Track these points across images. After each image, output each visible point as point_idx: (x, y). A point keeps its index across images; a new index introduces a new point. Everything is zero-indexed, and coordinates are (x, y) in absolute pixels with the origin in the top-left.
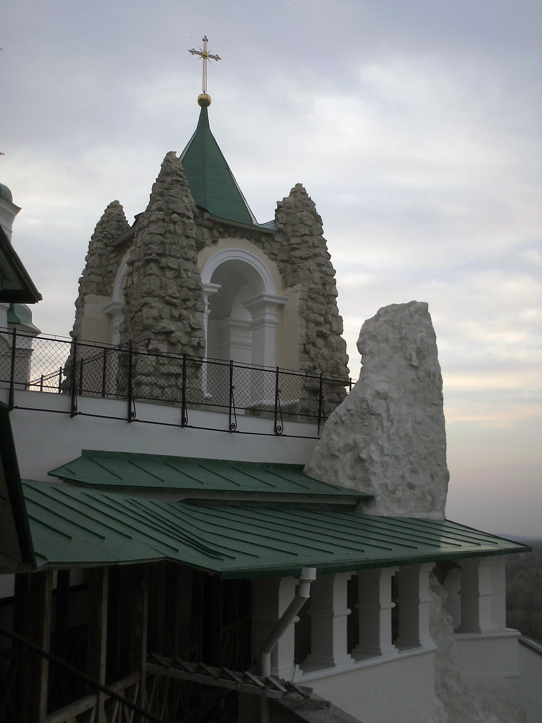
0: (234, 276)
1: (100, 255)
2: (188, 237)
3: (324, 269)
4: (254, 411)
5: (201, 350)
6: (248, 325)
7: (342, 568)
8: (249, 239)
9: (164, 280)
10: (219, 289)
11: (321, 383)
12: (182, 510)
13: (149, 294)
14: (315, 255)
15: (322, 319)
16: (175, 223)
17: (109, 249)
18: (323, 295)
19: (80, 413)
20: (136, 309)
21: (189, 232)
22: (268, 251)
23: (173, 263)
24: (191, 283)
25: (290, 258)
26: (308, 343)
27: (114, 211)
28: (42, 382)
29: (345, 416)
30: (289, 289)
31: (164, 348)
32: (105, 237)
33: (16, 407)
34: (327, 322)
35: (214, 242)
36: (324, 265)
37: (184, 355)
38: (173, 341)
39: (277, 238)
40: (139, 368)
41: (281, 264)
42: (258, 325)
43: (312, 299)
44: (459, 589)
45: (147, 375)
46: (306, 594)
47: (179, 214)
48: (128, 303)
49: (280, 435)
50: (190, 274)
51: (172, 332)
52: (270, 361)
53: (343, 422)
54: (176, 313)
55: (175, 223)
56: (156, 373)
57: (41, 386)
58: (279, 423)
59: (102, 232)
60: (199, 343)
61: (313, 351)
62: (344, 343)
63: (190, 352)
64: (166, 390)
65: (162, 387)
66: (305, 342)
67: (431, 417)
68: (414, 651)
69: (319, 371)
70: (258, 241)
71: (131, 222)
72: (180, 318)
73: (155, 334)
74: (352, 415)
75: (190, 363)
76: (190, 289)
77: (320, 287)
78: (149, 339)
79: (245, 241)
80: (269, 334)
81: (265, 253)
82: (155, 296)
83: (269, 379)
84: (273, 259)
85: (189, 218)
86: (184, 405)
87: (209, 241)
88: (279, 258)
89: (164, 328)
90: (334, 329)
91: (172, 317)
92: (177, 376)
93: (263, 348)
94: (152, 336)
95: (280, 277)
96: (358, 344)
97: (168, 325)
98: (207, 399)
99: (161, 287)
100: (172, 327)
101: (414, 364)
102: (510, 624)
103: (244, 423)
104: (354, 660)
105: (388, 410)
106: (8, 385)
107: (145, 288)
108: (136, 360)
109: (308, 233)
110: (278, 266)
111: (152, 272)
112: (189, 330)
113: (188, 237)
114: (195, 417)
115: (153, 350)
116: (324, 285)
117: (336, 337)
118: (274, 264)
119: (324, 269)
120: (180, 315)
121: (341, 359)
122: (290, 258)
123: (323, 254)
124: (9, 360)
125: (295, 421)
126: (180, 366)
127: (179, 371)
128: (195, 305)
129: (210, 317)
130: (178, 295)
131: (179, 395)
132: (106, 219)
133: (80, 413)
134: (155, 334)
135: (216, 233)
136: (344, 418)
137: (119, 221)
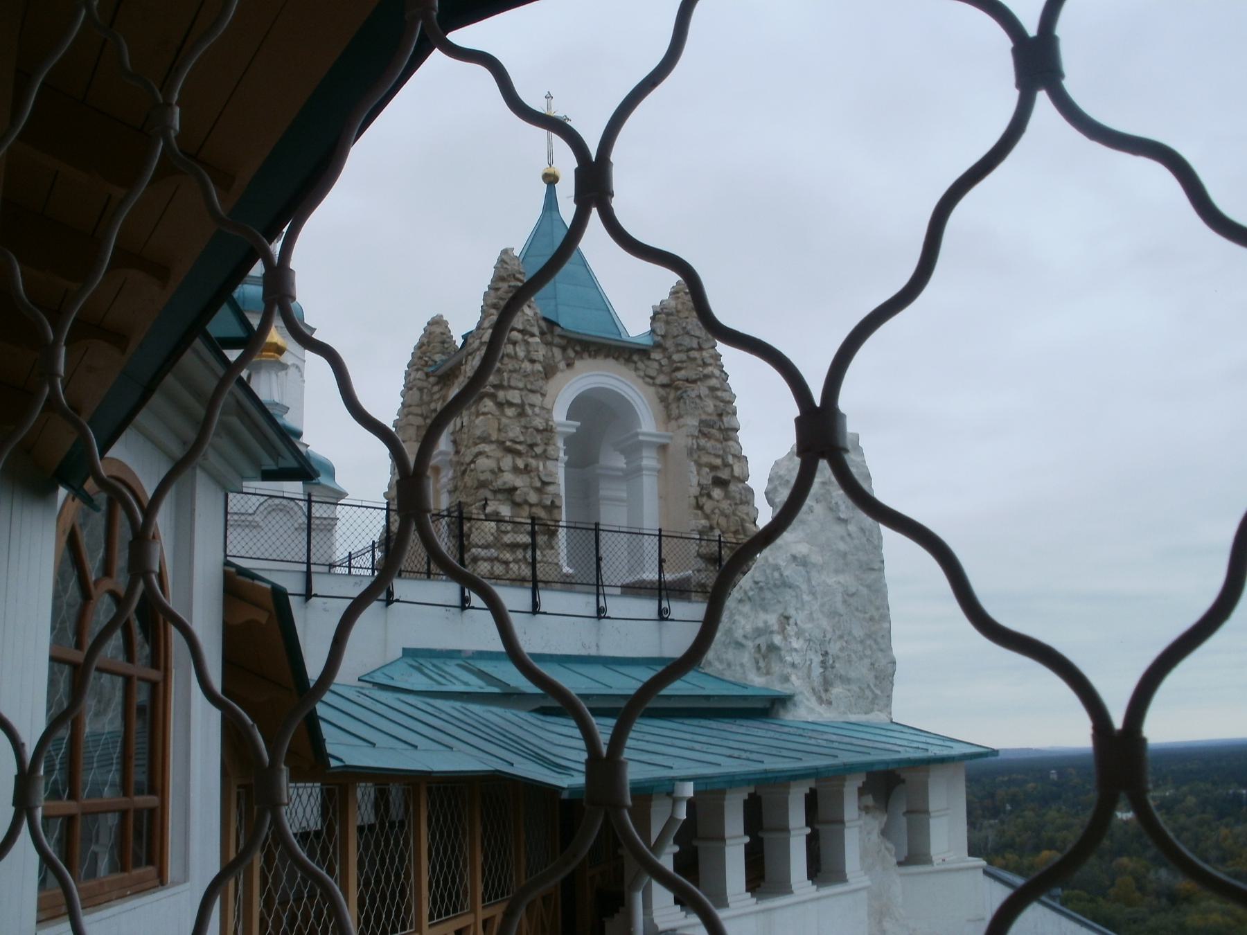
0: (596, 412)
1: (421, 390)
2: (533, 361)
3: (719, 394)
4: (634, 589)
5: (556, 511)
6: (620, 474)
7: (732, 781)
8: (617, 359)
9: (504, 420)
10: (577, 429)
11: (720, 548)
12: (539, 723)
13: (485, 439)
14: (707, 377)
15: (718, 462)
16: (514, 343)
17: (432, 379)
18: (720, 429)
19: (398, 601)
20: (468, 459)
21: (534, 356)
22: (642, 374)
23: (514, 396)
24: (539, 423)
25: (673, 381)
26: (701, 495)
27: (436, 332)
28: (350, 561)
29: (751, 589)
30: (673, 423)
31: (506, 511)
32: (426, 364)
33: (316, 595)
34: (726, 465)
35: (569, 365)
36: (717, 389)
37: (533, 519)
38: (518, 499)
39: (653, 355)
40: (475, 538)
41: (660, 390)
42: (634, 473)
43: (705, 435)
44: (904, 809)
45: (486, 547)
46: (682, 814)
47: (519, 331)
48: (457, 452)
49: (667, 619)
50: (537, 410)
51: (515, 489)
52: (650, 520)
53: (749, 599)
54: (520, 463)
55: (514, 343)
56: (497, 543)
57: (350, 567)
58: (665, 604)
59: (421, 358)
60: (553, 502)
61: (708, 506)
62: (750, 491)
63: (542, 513)
64: (511, 565)
65: (506, 563)
66: (697, 493)
67: (869, 587)
68: (838, 888)
69: (717, 532)
70: (629, 360)
71: (459, 342)
72: (527, 470)
73: (495, 492)
74: (761, 589)
75: (541, 529)
76: (538, 430)
77: (715, 418)
78: (486, 500)
79: (611, 362)
80: (649, 485)
81: (639, 376)
82: (492, 442)
83: (650, 545)
84: (648, 384)
85: (533, 335)
86: (535, 585)
87: (562, 365)
88: (658, 381)
89: (505, 483)
90: (736, 474)
91: (516, 470)
92: (524, 547)
93: (643, 506)
94: (489, 495)
95: (661, 407)
96: (766, 493)
97: (509, 478)
98: (567, 576)
99: (499, 430)
100: (519, 481)
101: (842, 516)
102: (973, 851)
103: (617, 606)
104: (754, 900)
105: (809, 580)
106: (304, 568)
107: (478, 432)
108: (470, 529)
109: (695, 345)
110: (657, 393)
111: (486, 410)
112: (538, 484)
113: (533, 361)
114: (548, 599)
115: (491, 514)
116: (720, 415)
117: (740, 485)
118: (652, 390)
119: (719, 394)
120: (526, 466)
121: (747, 514)
122: (673, 381)
123: (717, 372)
124: (304, 535)
125: (689, 600)
126: (528, 533)
127: (526, 539)
128: (545, 451)
129: (568, 465)
130: (522, 439)
131: (526, 571)
132: (425, 341)
133: (398, 601)
134: (495, 492)
135: (571, 353)
136: (751, 593)
137: (443, 342)
